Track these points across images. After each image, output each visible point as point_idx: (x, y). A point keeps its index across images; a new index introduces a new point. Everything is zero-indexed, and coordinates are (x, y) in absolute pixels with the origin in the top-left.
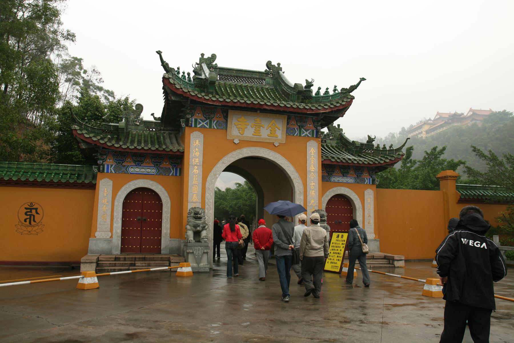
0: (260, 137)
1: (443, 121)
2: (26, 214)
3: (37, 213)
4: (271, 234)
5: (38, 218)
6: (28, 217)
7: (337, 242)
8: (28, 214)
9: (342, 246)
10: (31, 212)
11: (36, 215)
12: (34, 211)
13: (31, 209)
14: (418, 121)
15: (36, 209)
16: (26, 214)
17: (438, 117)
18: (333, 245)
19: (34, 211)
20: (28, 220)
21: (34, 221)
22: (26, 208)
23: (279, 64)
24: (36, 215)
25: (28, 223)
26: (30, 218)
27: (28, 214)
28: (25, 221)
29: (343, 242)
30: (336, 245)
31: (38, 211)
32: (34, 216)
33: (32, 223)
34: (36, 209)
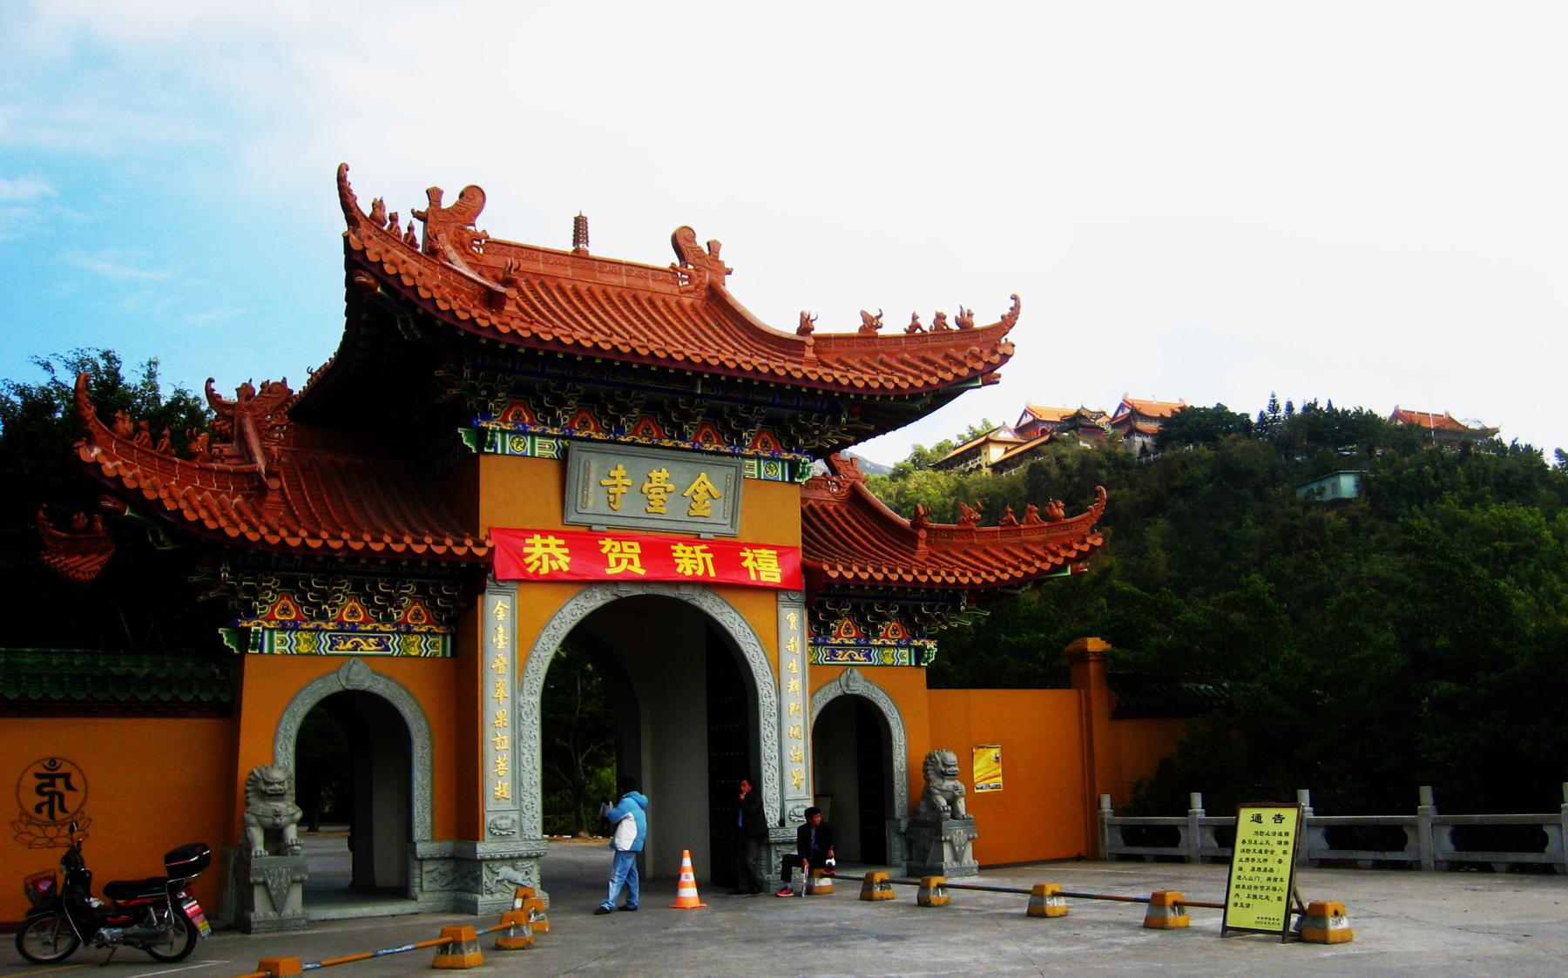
0: (673, 507)
1: (1044, 432)
2: (39, 790)
3: (69, 787)
4: (1402, 850)
5: (72, 800)
6: (46, 799)
7: (1259, 839)
8: (46, 789)
9: (1279, 849)
10: (52, 784)
11: (68, 794)
12: (60, 783)
13: (52, 778)
14: (1298, 394)
15: (67, 776)
16: (39, 790)
17: (1029, 419)
18: (1246, 847)
19: (60, 783)
20: (45, 809)
21: (63, 809)
22: (38, 776)
23: (681, 242)
24: (68, 794)
25: (45, 816)
26: (51, 803)
27: (46, 789)
28: (39, 809)
29: (1284, 839)
30: (1258, 847)
31: (74, 781)
32: (61, 797)
33: (59, 815)
34: (67, 776)
